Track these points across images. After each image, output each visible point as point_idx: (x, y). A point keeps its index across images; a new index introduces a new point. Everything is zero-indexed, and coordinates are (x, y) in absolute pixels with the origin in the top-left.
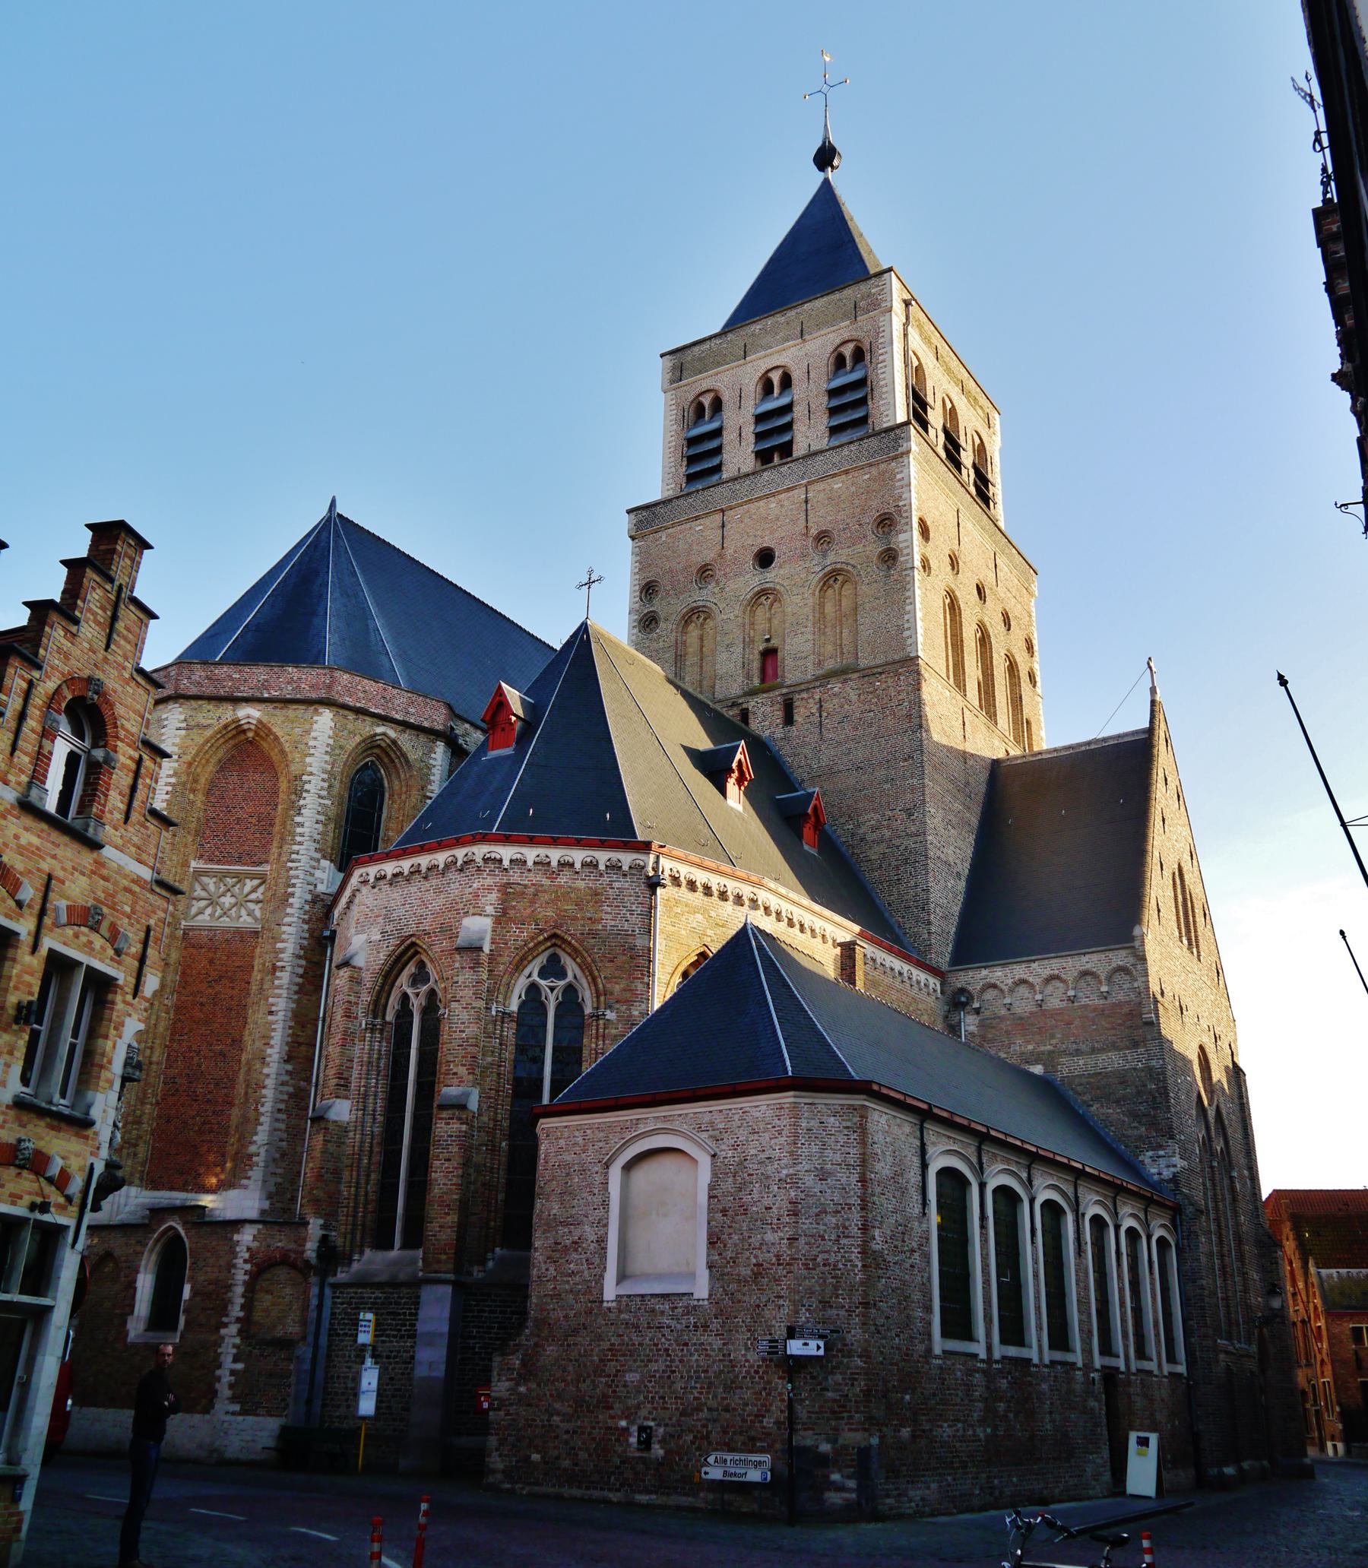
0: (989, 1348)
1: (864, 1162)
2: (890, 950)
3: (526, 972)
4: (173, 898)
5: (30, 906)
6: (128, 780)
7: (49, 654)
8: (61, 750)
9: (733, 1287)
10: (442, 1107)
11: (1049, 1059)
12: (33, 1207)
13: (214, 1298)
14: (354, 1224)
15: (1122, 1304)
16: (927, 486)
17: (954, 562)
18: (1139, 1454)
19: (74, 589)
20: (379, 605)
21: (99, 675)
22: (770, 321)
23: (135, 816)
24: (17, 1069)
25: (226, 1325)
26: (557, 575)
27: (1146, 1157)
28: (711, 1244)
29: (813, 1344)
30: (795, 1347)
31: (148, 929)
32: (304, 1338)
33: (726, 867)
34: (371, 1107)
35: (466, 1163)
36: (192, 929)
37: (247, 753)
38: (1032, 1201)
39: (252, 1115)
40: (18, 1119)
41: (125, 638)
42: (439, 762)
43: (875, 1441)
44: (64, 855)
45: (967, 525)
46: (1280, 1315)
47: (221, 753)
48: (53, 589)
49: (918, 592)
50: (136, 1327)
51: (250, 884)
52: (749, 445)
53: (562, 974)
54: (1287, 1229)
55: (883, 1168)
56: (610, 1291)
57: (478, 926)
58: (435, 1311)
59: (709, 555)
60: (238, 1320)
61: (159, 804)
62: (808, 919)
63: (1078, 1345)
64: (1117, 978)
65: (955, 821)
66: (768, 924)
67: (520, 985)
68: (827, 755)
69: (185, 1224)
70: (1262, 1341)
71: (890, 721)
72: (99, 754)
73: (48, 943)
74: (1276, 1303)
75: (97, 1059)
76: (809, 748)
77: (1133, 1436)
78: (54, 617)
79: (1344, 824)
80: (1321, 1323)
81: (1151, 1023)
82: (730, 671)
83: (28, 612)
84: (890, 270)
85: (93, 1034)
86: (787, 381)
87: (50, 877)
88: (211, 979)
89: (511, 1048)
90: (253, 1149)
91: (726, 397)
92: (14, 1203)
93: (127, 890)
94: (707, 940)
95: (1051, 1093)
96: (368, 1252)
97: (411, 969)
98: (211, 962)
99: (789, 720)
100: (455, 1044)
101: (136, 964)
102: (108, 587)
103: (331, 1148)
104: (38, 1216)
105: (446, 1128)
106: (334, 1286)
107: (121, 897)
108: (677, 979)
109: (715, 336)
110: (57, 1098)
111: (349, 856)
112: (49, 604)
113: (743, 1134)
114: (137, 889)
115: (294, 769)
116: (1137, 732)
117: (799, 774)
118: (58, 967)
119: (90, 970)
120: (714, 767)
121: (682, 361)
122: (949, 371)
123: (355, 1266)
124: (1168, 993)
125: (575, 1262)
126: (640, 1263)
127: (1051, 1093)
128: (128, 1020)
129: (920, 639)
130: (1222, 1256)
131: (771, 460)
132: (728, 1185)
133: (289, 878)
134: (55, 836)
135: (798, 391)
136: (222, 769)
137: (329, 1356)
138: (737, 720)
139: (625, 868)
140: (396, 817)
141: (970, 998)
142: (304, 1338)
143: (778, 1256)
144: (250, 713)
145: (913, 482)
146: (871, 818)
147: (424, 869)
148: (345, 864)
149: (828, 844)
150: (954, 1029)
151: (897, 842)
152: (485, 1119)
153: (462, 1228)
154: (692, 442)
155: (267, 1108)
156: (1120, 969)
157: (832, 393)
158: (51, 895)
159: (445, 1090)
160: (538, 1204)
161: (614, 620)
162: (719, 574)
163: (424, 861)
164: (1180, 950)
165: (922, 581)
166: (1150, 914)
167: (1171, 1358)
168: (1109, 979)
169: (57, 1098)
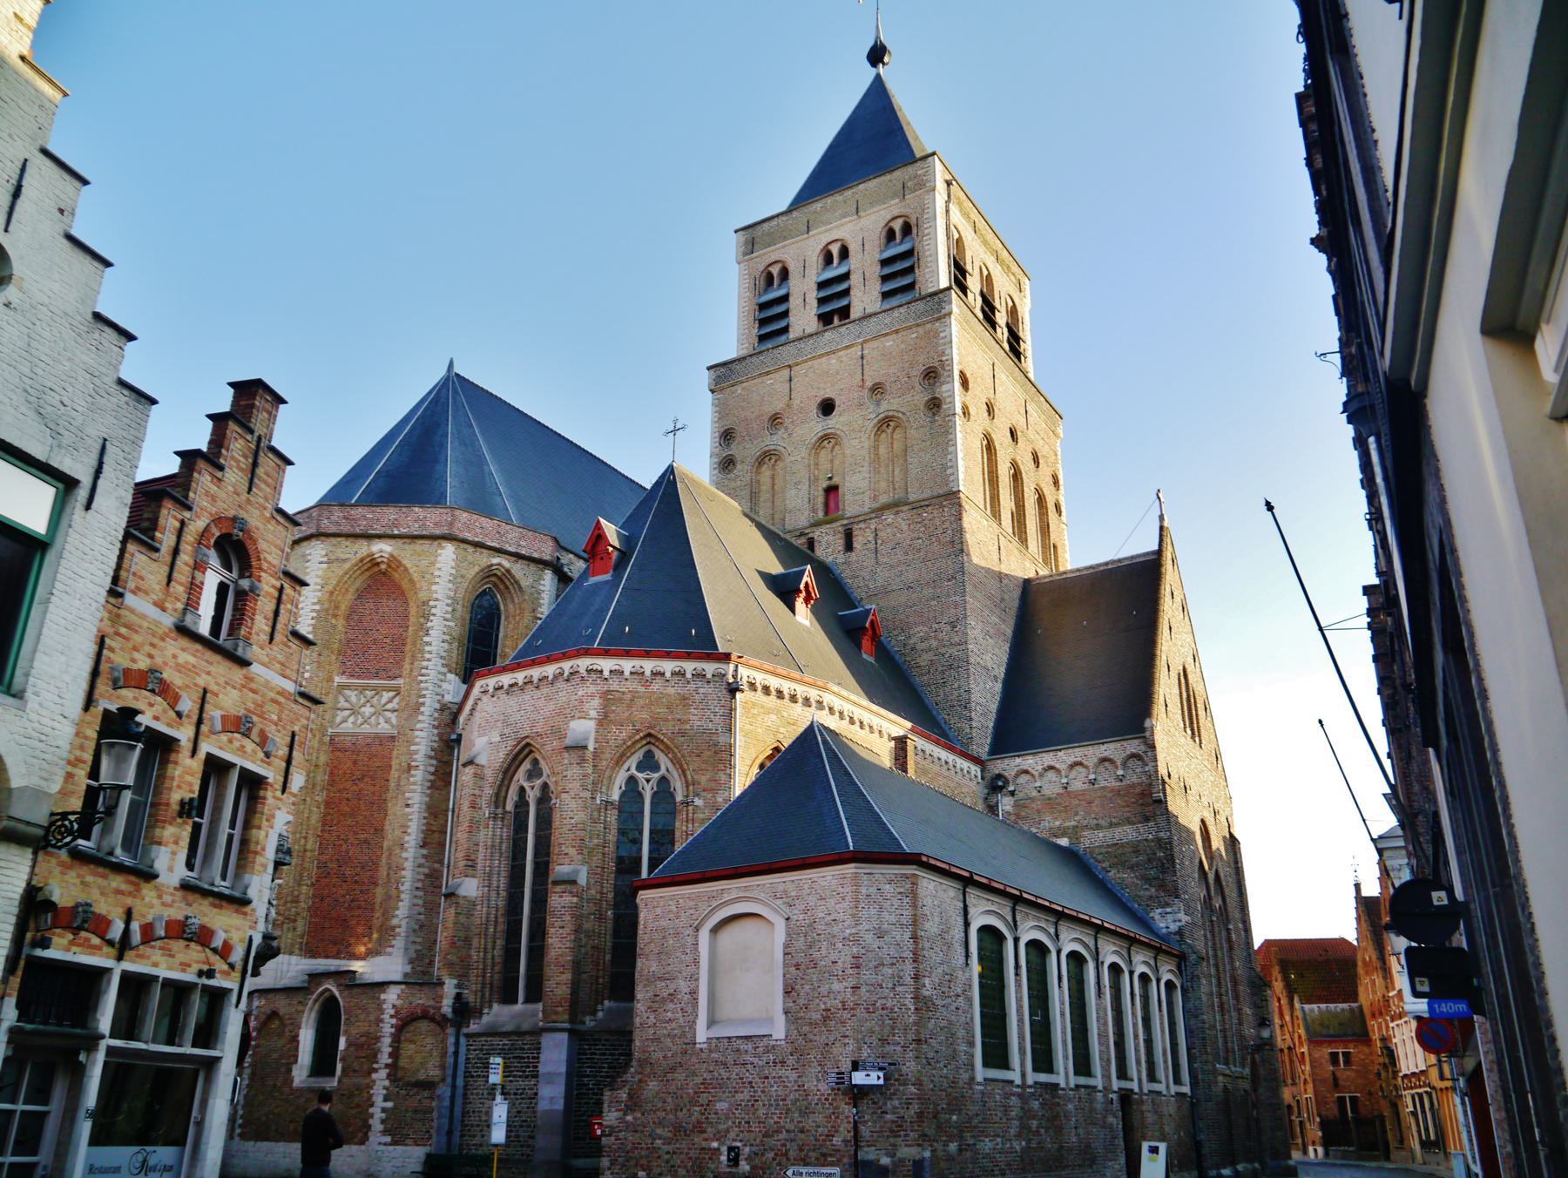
0: (1023, 1075)
1: (915, 923)
2: (938, 743)
3: (626, 767)
4: (313, 707)
5: (188, 716)
6: (271, 606)
7: (197, 496)
8: (211, 581)
9: (806, 1029)
10: (556, 883)
11: (1074, 833)
12: (200, 974)
13: (366, 1048)
14: (483, 984)
15: (1136, 1036)
16: (967, 344)
17: (990, 409)
18: (1151, 1160)
19: (218, 441)
20: (491, 450)
21: (243, 514)
22: (829, 200)
23: (278, 637)
24: (182, 856)
25: (376, 1071)
26: (650, 428)
27: (1156, 914)
28: (787, 993)
29: (874, 1075)
30: (859, 1078)
31: (293, 735)
32: (443, 1080)
33: (796, 674)
34: (495, 884)
35: (577, 931)
36: (338, 734)
37: (380, 581)
38: (1059, 952)
39: (393, 892)
40: (184, 898)
41: (265, 483)
42: (547, 588)
43: (927, 1154)
44: (217, 671)
45: (1002, 376)
46: (1266, 1045)
47: (358, 584)
48: (200, 439)
49: (959, 435)
50: (300, 1073)
51: (386, 696)
52: (813, 309)
53: (656, 768)
54: (1276, 972)
55: (931, 927)
56: (702, 1034)
57: (583, 728)
58: (554, 1054)
59: (779, 406)
60: (387, 1066)
61: (305, 629)
62: (867, 718)
63: (1099, 1075)
64: (1131, 763)
65: (992, 631)
66: (832, 722)
67: (621, 778)
68: (883, 576)
69: (339, 986)
70: (1253, 1062)
71: (936, 547)
72: (245, 584)
73: (205, 748)
74: (1266, 1034)
75: (252, 847)
76: (871, 572)
77: (1145, 1146)
78: (201, 464)
79: (1321, 629)
80: (1305, 1049)
81: (1160, 801)
82: (798, 506)
83: (178, 460)
84: (934, 154)
85: (247, 825)
86: (845, 253)
87: (205, 691)
88: (355, 778)
89: (614, 832)
90: (395, 922)
91: (791, 269)
92: (183, 971)
93: (273, 701)
94: (780, 737)
95: (1074, 859)
96: (495, 1006)
97: (526, 765)
98: (355, 762)
99: (849, 547)
100: (565, 829)
101: (284, 764)
102: (249, 437)
103: (462, 919)
104: (205, 981)
105: (559, 901)
106: (467, 1036)
107: (269, 707)
108: (755, 770)
109: (782, 214)
110: (218, 881)
111: (472, 670)
112: (196, 453)
113: (812, 900)
114: (282, 700)
115: (422, 595)
116: (1147, 554)
117: (858, 594)
118: (215, 768)
119: (244, 771)
120: (785, 589)
121: (753, 236)
122: (985, 243)
123: (485, 1019)
124: (1174, 776)
125: (671, 1011)
126: (725, 1011)
127: (1074, 859)
128: (278, 813)
129: (961, 476)
130: (1220, 995)
131: (831, 322)
132: (800, 943)
133: (420, 689)
134: (209, 655)
135: (854, 262)
136: (359, 597)
137: (465, 1095)
138: (805, 548)
139: (709, 676)
140: (511, 637)
141: (1006, 782)
142: (443, 1080)
143: (843, 1003)
144: (382, 548)
145: (955, 340)
146: (920, 631)
147: (535, 680)
148: (468, 678)
149: (882, 652)
150: (993, 809)
151: (943, 650)
152: (593, 892)
153: (575, 985)
154: (763, 307)
155: (406, 886)
156: (1133, 756)
157: (885, 263)
158: (207, 707)
159: (558, 868)
160: (639, 964)
161: (696, 463)
162: (787, 421)
163: (536, 673)
164: (1184, 739)
165: (963, 425)
166: (1158, 709)
167: (1178, 1081)
168: (1124, 764)
169: (218, 881)
